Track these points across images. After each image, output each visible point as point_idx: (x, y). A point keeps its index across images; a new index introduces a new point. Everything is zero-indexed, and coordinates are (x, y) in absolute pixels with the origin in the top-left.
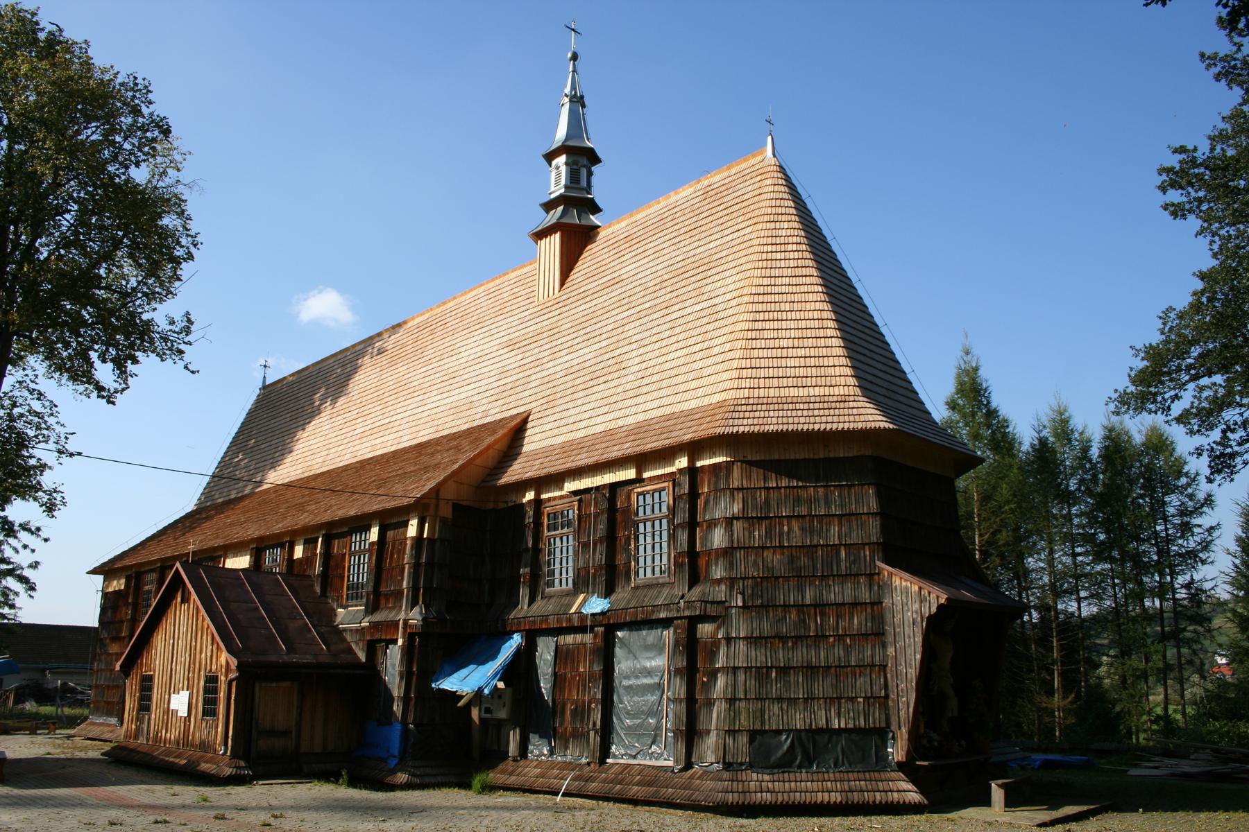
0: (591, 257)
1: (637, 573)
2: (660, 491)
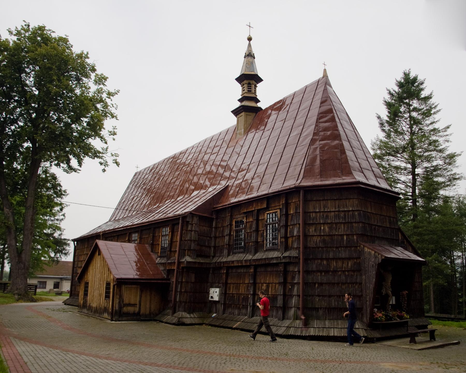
0: (377, 122)
1: (266, 245)
2: (275, 213)
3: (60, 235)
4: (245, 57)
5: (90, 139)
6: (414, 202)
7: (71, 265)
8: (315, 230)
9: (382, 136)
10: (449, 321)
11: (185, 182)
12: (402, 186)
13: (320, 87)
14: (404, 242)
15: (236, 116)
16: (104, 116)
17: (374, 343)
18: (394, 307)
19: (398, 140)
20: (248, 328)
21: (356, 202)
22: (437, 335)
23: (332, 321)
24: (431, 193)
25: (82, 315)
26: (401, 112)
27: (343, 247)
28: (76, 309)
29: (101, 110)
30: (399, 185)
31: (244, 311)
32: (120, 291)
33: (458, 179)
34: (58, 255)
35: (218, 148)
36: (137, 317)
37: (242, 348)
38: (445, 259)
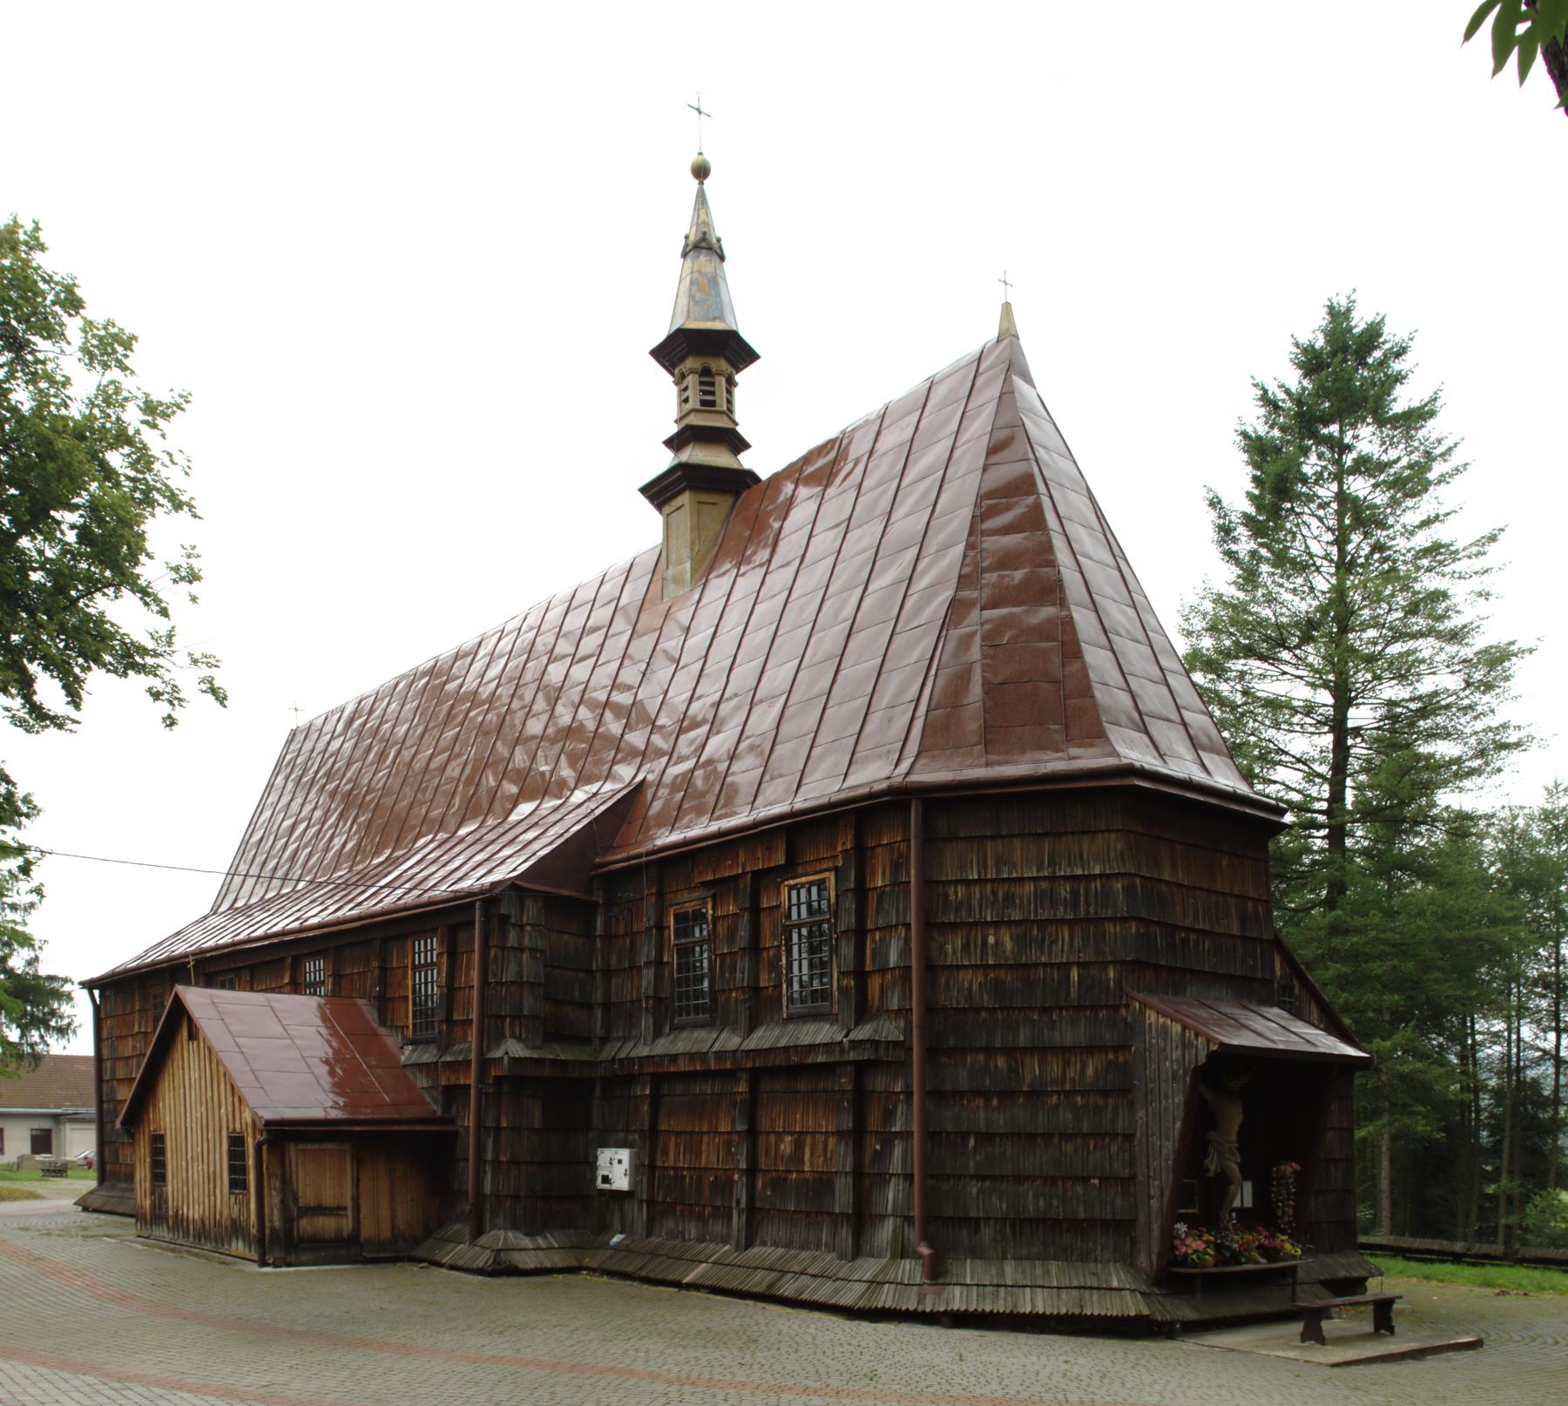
3: (30, 963)
4: (684, 255)
5: (98, 596)
6: (1337, 835)
7: (91, 1069)
8: (966, 947)
9: (1224, 578)
10: (1443, 1261)
11: (482, 766)
12: (1293, 777)
13: (987, 384)
14: (1292, 988)
15: (659, 507)
16: (141, 502)
17: (1173, 1338)
18: (1248, 1219)
19: (1287, 596)
20: (734, 1285)
21: (1117, 844)
22: (1401, 1312)
23: (1027, 1264)
24: (1403, 804)
25: (153, 1246)
26: (1304, 480)
27: (1067, 1009)
28: (129, 1227)
29: (128, 478)
30: (1280, 773)
31: (718, 1228)
32: (282, 1164)
33: (1518, 745)
34: (35, 1035)
35: (597, 638)
36: (349, 1250)
37: (717, 1354)
38: (1440, 1045)
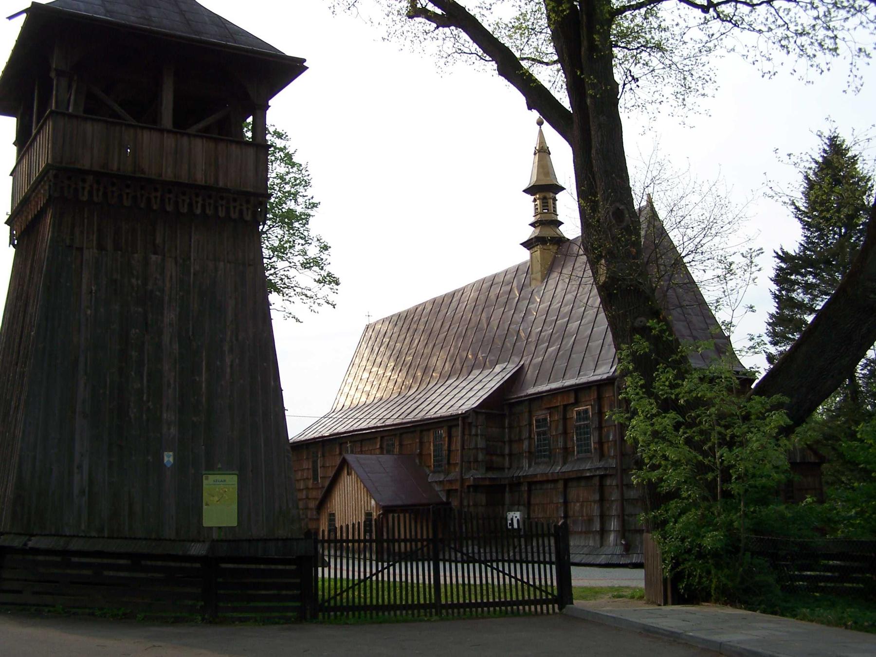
4: (535, 154)
